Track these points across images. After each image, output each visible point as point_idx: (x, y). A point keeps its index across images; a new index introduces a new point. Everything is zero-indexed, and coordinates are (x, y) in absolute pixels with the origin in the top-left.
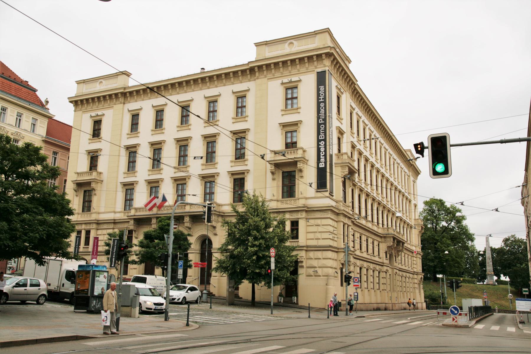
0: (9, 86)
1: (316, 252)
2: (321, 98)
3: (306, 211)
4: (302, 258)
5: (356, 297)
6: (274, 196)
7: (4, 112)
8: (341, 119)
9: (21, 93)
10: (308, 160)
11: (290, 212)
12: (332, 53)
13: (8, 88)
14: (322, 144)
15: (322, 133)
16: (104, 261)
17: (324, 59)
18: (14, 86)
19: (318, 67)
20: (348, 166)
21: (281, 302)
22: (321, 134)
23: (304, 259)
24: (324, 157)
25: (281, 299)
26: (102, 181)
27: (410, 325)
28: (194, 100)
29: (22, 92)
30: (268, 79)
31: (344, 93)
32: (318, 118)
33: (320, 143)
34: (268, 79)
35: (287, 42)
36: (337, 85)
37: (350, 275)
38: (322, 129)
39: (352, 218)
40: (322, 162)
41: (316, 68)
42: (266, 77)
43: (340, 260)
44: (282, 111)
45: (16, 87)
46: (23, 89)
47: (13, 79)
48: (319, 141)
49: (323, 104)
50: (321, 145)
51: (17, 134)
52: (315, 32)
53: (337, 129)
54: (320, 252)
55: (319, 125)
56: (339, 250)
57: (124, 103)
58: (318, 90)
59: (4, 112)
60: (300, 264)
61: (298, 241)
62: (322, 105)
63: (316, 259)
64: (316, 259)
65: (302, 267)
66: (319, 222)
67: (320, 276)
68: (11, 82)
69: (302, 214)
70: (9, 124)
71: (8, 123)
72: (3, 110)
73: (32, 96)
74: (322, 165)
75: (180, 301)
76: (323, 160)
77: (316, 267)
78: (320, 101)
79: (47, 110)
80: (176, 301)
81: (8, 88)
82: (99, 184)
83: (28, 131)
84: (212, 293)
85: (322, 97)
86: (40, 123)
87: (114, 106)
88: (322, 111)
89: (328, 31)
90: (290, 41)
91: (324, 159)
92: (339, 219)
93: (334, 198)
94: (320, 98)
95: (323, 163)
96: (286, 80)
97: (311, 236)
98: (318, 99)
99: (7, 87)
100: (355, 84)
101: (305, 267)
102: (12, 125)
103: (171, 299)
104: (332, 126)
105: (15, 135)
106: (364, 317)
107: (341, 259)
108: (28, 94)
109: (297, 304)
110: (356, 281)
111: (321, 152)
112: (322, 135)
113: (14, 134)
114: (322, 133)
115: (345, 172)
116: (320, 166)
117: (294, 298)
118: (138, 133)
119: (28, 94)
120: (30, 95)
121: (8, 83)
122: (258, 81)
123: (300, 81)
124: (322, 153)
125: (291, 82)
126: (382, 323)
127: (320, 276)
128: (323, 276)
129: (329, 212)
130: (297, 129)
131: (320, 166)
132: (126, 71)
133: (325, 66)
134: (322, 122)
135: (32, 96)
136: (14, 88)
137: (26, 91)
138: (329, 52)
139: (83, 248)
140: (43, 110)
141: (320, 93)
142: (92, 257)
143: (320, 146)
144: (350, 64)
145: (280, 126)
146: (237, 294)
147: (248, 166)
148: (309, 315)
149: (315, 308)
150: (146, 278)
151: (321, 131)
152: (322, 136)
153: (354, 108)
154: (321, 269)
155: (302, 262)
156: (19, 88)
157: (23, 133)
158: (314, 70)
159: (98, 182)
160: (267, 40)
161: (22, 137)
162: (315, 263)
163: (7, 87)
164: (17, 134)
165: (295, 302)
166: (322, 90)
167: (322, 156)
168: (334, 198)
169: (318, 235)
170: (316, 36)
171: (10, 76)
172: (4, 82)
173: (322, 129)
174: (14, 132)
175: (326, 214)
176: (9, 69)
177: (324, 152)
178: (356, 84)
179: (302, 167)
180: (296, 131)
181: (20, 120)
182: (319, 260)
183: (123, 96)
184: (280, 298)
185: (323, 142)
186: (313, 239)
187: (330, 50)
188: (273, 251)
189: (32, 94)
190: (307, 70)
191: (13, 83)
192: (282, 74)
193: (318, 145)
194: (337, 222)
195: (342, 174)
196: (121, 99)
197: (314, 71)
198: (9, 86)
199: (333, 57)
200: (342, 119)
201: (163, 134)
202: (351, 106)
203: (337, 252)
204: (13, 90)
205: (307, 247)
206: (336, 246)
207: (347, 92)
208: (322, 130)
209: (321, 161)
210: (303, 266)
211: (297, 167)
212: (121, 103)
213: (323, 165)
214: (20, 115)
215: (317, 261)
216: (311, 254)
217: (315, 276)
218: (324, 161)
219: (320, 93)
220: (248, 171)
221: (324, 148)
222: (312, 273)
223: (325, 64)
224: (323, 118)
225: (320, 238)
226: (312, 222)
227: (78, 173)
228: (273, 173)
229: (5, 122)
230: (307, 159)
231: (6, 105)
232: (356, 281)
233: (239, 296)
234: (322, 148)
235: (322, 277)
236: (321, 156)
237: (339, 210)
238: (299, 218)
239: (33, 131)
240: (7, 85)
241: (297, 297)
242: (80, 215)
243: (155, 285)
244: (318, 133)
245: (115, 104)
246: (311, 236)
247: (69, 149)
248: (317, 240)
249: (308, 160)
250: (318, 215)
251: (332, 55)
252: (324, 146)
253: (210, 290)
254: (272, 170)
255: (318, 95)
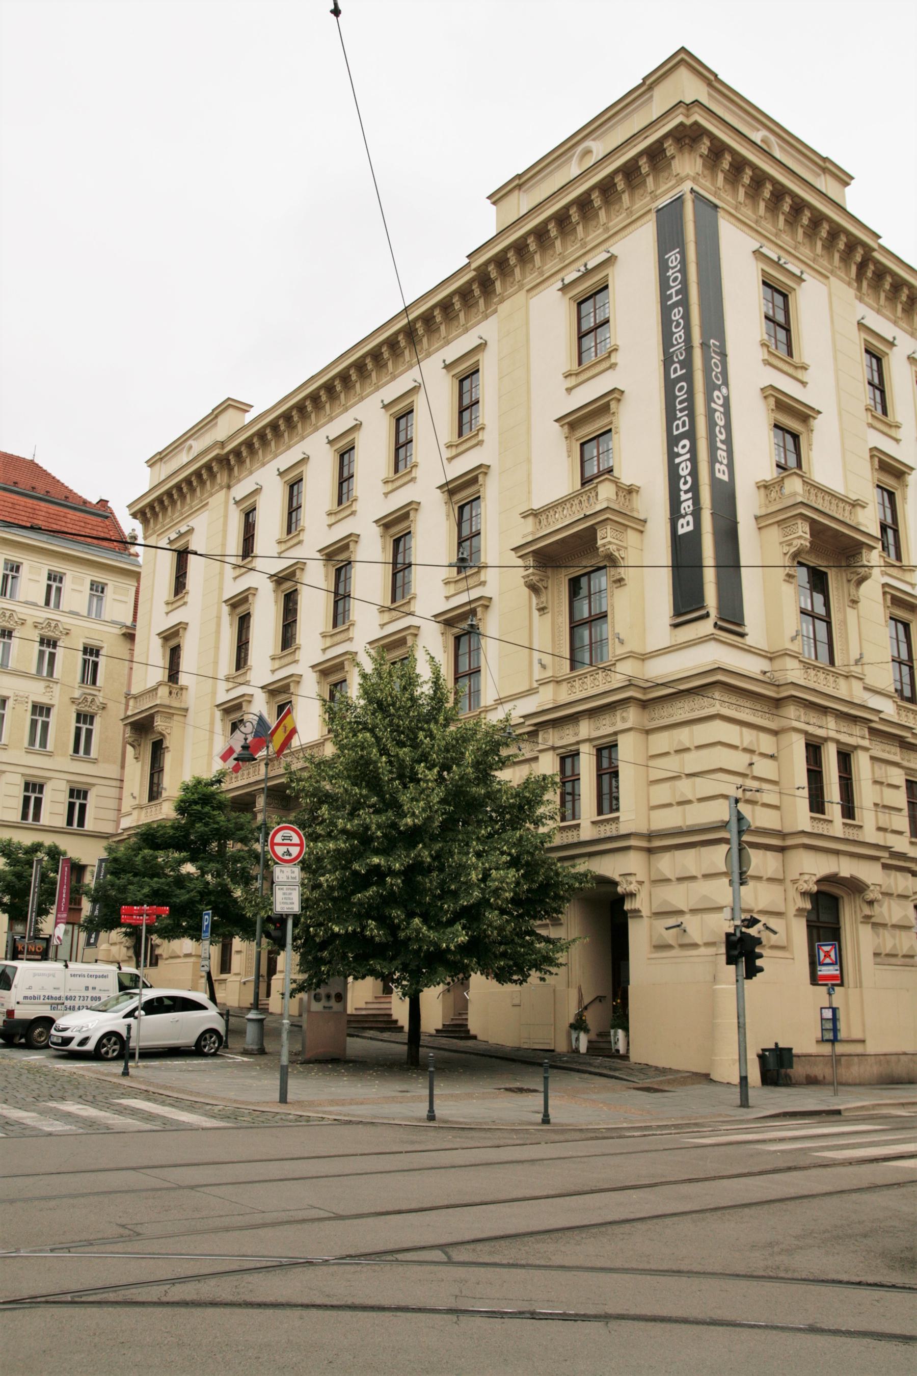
0: (30, 510)
1: (679, 854)
2: (673, 290)
3: (644, 704)
4: (630, 878)
5: (829, 1025)
6: (134, 798)
7: (14, 574)
8: (796, 368)
9: (63, 524)
10: (645, 521)
11: (592, 713)
12: (696, 123)
13: (27, 514)
14: (682, 451)
15: (681, 410)
16: (694, 874)
17: (673, 158)
18: (45, 509)
19: (658, 192)
20: (801, 514)
21: (577, 1051)
22: (679, 415)
23: (641, 883)
24: (690, 495)
25: (577, 1039)
26: (186, 710)
27: (897, 1168)
28: (488, 343)
29: (68, 521)
30: (528, 291)
31: (804, 276)
32: (668, 361)
33: (676, 450)
34: (528, 291)
35: (573, 155)
36: (756, 246)
37: (753, 931)
38: (681, 395)
39: (871, 721)
40: (686, 514)
41: (655, 198)
42: (521, 288)
43: (794, 882)
44: (569, 378)
45: (50, 511)
46: (69, 516)
47: (43, 492)
48: (672, 441)
49: (680, 308)
50: (679, 455)
51: (49, 625)
52: (825, 159)
53: (765, 397)
54: (691, 853)
55: (669, 385)
56: (789, 842)
57: (229, 487)
58: (663, 266)
59: (14, 574)
60: (627, 906)
61: (618, 818)
62: (677, 315)
63: (680, 879)
64: (680, 879)
65: (637, 913)
66: (684, 736)
67: (695, 946)
68: (35, 502)
69: (625, 714)
70: (26, 603)
71: (67, 610)
72: (12, 570)
73: (96, 528)
74: (685, 527)
75: (90, 1046)
76: (687, 506)
77: (680, 912)
78: (669, 303)
79: (132, 557)
80: (73, 1046)
81: (27, 514)
82: (175, 717)
83: (82, 614)
84: (396, 1021)
85: (675, 286)
86: (114, 593)
87: (210, 500)
88: (677, 335)
89: (682, 60)
90: (580, 148)
91: (690, 502)
92: (785, 723)
93: (749, 640)
94: (669, 293)
95: (690, 518)
96: (571, 276)
97: (662, 794)
98: (664, 297)
99: (23, 513)
100: (868, 249)
101: (645, 912)
102: (35, 604)
103: (60, 1041)
104: (726, 383)
105: (42, 628)
106: (838, 1112)
107: (797, 877)
108: (83, 524)
109: (626, 1057)
110: (828, 961)
111: (682, 480)
112: (679, 419)
113: (40, 626)
114: (681, 410)
115: (795, 542)
116: (681, 531)
117: (616, 1034)
118: (410, 599)
119: (83, 524)
120: (90, 526)
121: (28, 505)
122: (504, 308)
123: (611, 260)
124: (685, 483)
125: (588, 273)
126: (760, 1153)
127: (695, 946)
128: (707, 944)
129: (717, 695)
130: (611, 423)
131: (681, 531)
132: (229, 399)
133: (681, 180)
134: (679, 373)
135: (96, 528)
136: (43, 514)
137: (77, 518)
138: (681, 124)
139: (593, 823)
140: (119, 559)
141: (669, 277)
142: (57, 918)
143: (677, 461)
144: (847, 189)
145: (562, 426)
146: (464, 1023)
147: (487, 585)
148: (431, 1110)
149: (678, 1071)
150: (16, 968)
151: (679, 407)
152: (680, 422)
153: (891, 340)
154: (696, 919)
155: (632, 895)
156: (56, 512)
157: (66, 621)
158: (648, 208)
159: (173, 714)
160: (520, 172)
161: (65, 631)
162: (676, 896)
163: (23, 513)
164: (49, 625)
165: (618, 1051)
166: (675, 264)
167: (686, 492)
168: (749, 640)
169: (685, 788)
170: (651, 97)
171: (33, 488)
172: (15, 502)
173: (681, 395)
174: (40, 621)
175: (706, 702)
176: (49, 474)
177: (689, 479)
178: (874, 250)
179: (610, 543)
180: (610, 430)
181: (59, 590)
182: (693, 885)
183: (225, 467)
184: (574, 1036)
185: (686, 442)
186: (669, 805)
187: (688, 116)
188: (284, 838)
189: (95, 523)
190: (628, 216)
191: (43, 504)
192: (563, 259)
193: (672, 455)
194: (775, 733)
195: (785, 550)
196: (222, 478)
197: (650, 210)
198: (30, 510)
199: (706, 142)
200: (804, 368)
201: (299, 546)
202: (861, 326)
203: (782, 849)
204: (42, 518)
205: (650, 836)
206: (778, 828)
207: (832, 279)
208: (681, 402)
209: (683, 512)
210: (638, 911)
211: (598, 549)
212: (222, 488)
213: (688, 524)
214: (98, 589)
215: (684, 886)
216: (666, 864)
217: (682, 946)
218: (691, 508)
219: (669, 277)
220: (486, 603)
221: (689, 463)
222: (670, 937)
223: (679, 171)
224: (681, 358)
225: (690, 797)
226: (661, 742)
227: (535, 514)
228: (534, 588)
229: (103, 618)
230: (642, 517)
231: (16, 556)
232: (828, 961)
233: (469, 1031)
234: (683, 465)
235: (703, 950)
236: (682, 493)
237: (778, 686)
238: (616, 733)
239: (58, 607)
240: (25, 509)
241: (626, 1029)
242: (144, 811)
243: (56, 994)
244: (671, 416)
245: (211, 495)
246: (662, 794)
247: (134, 635)
248: (680, 808)
249: (645, 521)
250: (682, 711)
251: (701, 135)
252: (688, 456)
253: (393, 1012)
254: (528, 576)
255: (664, 284)
